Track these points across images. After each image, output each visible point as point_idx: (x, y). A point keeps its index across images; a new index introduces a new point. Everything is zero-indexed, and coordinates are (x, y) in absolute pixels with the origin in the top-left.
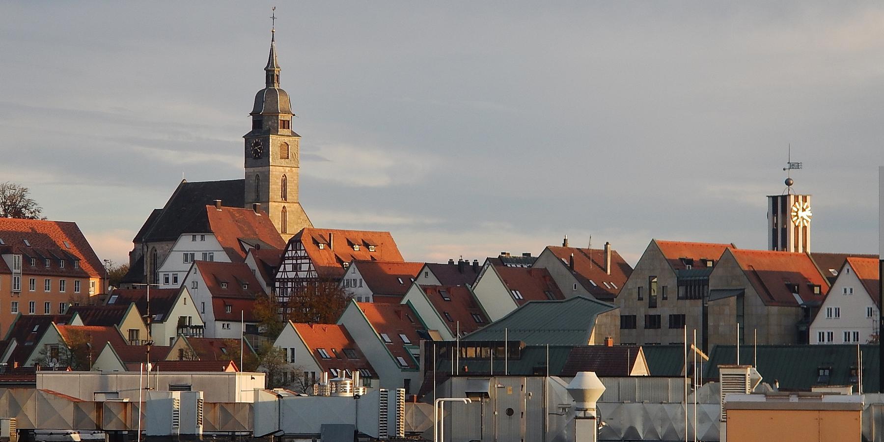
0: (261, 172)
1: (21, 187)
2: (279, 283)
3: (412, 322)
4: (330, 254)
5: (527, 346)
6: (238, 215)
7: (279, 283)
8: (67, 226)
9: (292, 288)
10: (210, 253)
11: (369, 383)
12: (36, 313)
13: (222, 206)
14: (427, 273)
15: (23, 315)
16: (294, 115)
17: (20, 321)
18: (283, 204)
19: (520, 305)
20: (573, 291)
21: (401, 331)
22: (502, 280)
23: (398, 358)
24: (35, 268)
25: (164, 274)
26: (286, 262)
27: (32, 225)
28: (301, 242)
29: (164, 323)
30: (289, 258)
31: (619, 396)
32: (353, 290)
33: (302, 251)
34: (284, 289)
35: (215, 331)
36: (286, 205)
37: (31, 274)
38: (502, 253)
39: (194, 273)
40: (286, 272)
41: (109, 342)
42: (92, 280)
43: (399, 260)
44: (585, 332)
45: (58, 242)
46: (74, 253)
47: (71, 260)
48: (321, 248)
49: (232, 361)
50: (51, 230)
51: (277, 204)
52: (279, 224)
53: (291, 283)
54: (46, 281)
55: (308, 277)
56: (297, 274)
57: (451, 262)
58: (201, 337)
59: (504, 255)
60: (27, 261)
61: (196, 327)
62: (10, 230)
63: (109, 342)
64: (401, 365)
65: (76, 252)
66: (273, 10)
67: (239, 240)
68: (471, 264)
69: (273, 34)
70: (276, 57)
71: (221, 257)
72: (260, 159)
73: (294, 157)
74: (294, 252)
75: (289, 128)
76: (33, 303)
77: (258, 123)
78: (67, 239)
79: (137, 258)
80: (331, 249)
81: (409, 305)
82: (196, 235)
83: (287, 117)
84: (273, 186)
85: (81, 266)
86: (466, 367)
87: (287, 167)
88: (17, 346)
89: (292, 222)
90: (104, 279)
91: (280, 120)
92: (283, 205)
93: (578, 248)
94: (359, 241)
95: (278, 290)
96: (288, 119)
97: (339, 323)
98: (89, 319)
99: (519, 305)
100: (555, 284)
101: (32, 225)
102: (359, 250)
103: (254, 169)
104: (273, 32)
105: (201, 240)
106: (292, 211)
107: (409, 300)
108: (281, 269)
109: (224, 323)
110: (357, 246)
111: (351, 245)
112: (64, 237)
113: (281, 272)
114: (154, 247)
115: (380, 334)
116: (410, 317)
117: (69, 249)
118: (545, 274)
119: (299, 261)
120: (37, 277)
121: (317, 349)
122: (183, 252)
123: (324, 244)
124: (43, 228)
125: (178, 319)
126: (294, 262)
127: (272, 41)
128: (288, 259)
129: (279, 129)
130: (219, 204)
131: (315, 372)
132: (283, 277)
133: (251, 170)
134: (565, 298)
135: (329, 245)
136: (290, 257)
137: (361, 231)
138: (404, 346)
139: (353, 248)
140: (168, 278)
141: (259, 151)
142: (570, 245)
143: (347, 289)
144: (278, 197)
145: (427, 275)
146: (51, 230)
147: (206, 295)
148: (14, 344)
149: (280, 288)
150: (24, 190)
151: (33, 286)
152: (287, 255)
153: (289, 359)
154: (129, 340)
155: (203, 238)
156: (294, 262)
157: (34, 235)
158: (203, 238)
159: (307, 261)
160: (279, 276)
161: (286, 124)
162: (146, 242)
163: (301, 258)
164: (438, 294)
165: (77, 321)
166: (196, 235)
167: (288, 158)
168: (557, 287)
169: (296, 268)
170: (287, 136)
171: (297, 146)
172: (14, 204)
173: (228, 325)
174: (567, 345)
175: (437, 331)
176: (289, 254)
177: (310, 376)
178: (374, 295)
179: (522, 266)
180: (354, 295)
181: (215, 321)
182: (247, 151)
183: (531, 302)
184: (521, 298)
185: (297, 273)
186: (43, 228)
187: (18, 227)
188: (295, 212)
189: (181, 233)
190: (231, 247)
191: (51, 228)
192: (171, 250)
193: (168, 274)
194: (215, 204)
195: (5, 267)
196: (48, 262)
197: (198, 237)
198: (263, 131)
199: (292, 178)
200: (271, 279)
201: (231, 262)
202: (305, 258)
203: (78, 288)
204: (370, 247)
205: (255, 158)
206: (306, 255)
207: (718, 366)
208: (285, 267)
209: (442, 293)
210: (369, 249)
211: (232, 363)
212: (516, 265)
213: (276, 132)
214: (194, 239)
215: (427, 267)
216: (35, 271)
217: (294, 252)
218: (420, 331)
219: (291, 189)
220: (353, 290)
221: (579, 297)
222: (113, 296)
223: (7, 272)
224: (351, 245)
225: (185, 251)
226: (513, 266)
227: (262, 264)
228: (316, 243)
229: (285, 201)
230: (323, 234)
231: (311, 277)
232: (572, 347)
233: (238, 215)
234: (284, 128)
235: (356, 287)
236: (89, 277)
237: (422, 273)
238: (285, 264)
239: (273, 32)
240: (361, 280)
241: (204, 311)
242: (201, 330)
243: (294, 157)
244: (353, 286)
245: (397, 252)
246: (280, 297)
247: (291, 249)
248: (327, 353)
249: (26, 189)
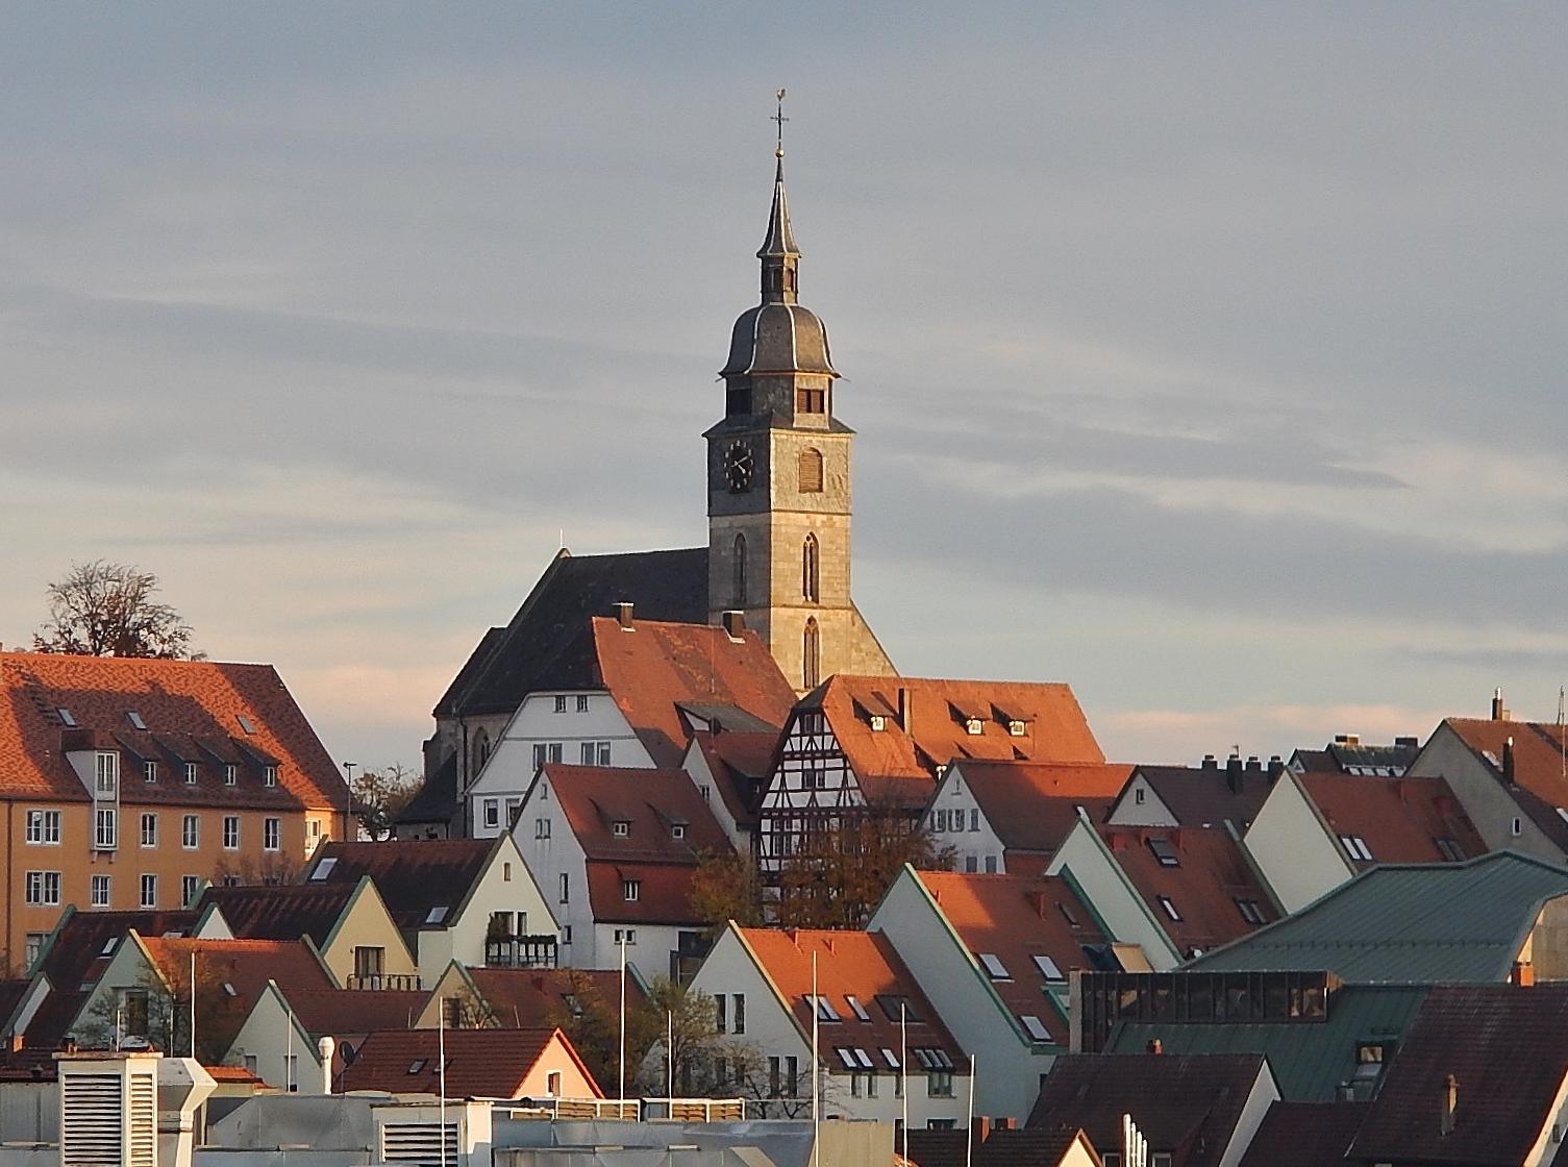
0: (746, 527)
1: (138, 575)
2: (769, 821)
3: (1072, 923)
4: (900, 745)
5: (1345, 986)
6: (679, 643)
7: (769, 821)
8: (251, 677)
9: (801, 834)
10: (602, 744)
11: (947, 1084)
12: (113, 906)
13: (634, 618)
14: (1140, 793)
15: (79, 910)
16: (837, 376)
17: (71, 928)
18: (808, 610)
19: (1360, 871)
20: (1512, 837)
21: (1040, 947)
22: (1317, 810)
23: (1024, 1018)
24: (157, 785)
25: (507, 800)
26: (788, 765)
27: (154, 673)
28: (823, 715)
29: (449, 928)
30: (792, 756)
31: (39, 1122)
32: (954, 838)
33: (826, 737)
34: (781, 837)
35: (594, 954)
36: (816, 614)
37: (149, 804)
38: (1338, 739)
39: (542, 798)
40: (849, 789)
41: (272, 982)
42: (311, 818)
43: (1090, 759)
44: (1505, 947)
45: (223, 716)
46: (265, 749)
47: (254, 764)
48: (875, 728)
49: (558, 1031)
50: (204, 685)
51: (791, 611)
52: (797, 665)
53: (799, 821)
54: (186, 819)
55: (841, 804)
56: (813, 798)
57: (1209, 763)
58: (551, 965)
59: (1343, 744)
60: (133, 766)
61: (536, 940)
62: (93, 686)
63: (272, 982)
64: (1031, 1037)
65: (271, 746)
66: (780, 98)
67: (679, 709)
68: (1264, 768)
69: (779, 160)
70: (786, 221)
71: (630, 755)
72: (748, 491)
73: (838, 486)
74: (806, 739)
75: (822, 411)
76: (152, 879)
77: (738, 400)
78: (248, 709)
79: (443, 758)
80: (903, 729)
81: (1066, 879)
82: (564, 697)
83: (818, 382)
84: (781, 565)
85: (283, 782)
86: (1158, 1043)
87: (817, 513)
88: (51, 991)
89: (833, 658)
90: (345, 813)
91: (800, 390)
92: (808, 613)
93: (1532, 721)
94: (984, 710)
95: (767, 838)
96: (821, 388)
97: (873, 928)
98: (248, 927)
99: (1356, 871)
100: (1465, 819)
101: (154, 673)
102: (983, 733)
103: (729, 518)
104: (779, 156)
105: (578, 711)
106: (833, 630)
107: (1065, 865)
108: (775, 785)
109: (619, 927)
110: (975, 722)
111: (960, 719)
112: (241, 705)
113: (773, 792)
114: (481, 729)
115: (976, 956)
116: (1066, 909)
117: (253, 738)
118: (1439, 794)
119: (819, 764)
120: (162, 810)
121: (804, 996)
122: (580, 742)
123: (884, 717)
124: (182, 681)
125: (489, 921)
126: (808, 765)
127: (778, 180)
128: (792, 759)
129: (795, 414)
130: (628, 614)
131: (795, 1058)
132: (779, 805)
133: (724, 522)
134: (1487, 851)
135: (899, 720)
136: (797, 752)
137: (990, 683)
138: (1044, 988)
139: (966, 728)
140: (495, 810)
141: (744, 471)
142: (1516, 715)
143: (938, 836)
144: (795, 593)
145: (1142, 799)
146: (204, 685)
147: (570, 854)
148: (43, 989)
149: (771, 834)
150: (144, 582)
151: (152, 835)
152: (787, 748)
153: (730, 1024)
154: (356, 975)
155: (582, 705)
156: (808, 765)
157: (156, 700)
158: (582, 705)
159: (839, 763)
160: (769, 802)
161: (814, 401)
162: (461, 715)
163: (824, 755)
164: (1144, 847)
165: (215, 928)
166: (564, 697)
167: (820, 490)
168: (1470, 828)
169: (811, 781)
170: (818, 431)
171: (846, 457)
172: (116, 620)
173: (629, 933)
174: (1425, 982)
175: (1138, 946)
176: (794, 744)
177: (784, 1068)
178: (1009, 851)
179: (1391, 772)
180: (956, 853)
181: (595, 922)
182: (712, 472)
183: (1380, 869)
184: (1368, 856)
185: (813, 796)
186: (182, 681)
187: (115, 679)
188: (842, 634)
189: (528, 692)
190: (657, 726)
191: (204, 680)
192: (502, 738)
193: (496, 801)
194: (617, 613)
195: (75, 787)
196: (192, 774)
197: (571, 702)
198: (754, 419)
199: (832, 542)
200: (749, 813)
201: (655, 767)
202: (834, 754)
203: (275, 838)
204: (1012, 724)
205: (734, 491)
206: (836, 747)
207: (55, 1055)
208: (783, 779)
209: (1153, 844)
210: (1009, 730)
211: (558, 1036)
212: (1374, 770)
213: (789, 422)
214: (560, 707)
215: (1140, 776)
216: (156, 793)
217: (806, 739)
218: (1090, 946)
219: (829, 572)
220: (954, 838)
221: (1505, 854)
222: (324, 860)
223: (84, 798)
224: (960, 719)
225: (535, 739)
226: (1368, 772)
227: (726, 772)
228: (864, 716)
229: (815, 605)
230: (885, 690)
231: (848, 804)
232: (1429, 988)
233: (679, 643)
234: (809, 411)
235: (962, 830)
236: (303, 810)
237: (1129, 793)
238: (783, 772)
239: (779, 156)
240: (974, 812)
241: (566, 897)
242: (551, 948)
243: (838, 486)
244: (954, 828)
245: (1087, 734)
246: (772, 857)
247: (798, 732)
248: (832, 1007)
249: (148, 579)
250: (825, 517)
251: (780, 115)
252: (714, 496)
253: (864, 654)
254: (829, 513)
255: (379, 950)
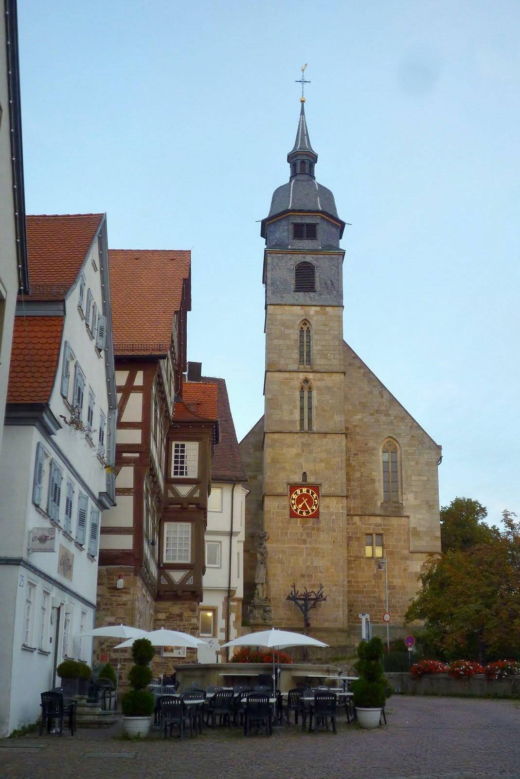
18: (301, 374)
36: (310, 376)
51: (287, 375)
92: (302, 376)
250: (318, 309)
251: (306, 82)
252: (269, 260)
253: (393, 418)
254: (322, 306)
255: (190, 251)
